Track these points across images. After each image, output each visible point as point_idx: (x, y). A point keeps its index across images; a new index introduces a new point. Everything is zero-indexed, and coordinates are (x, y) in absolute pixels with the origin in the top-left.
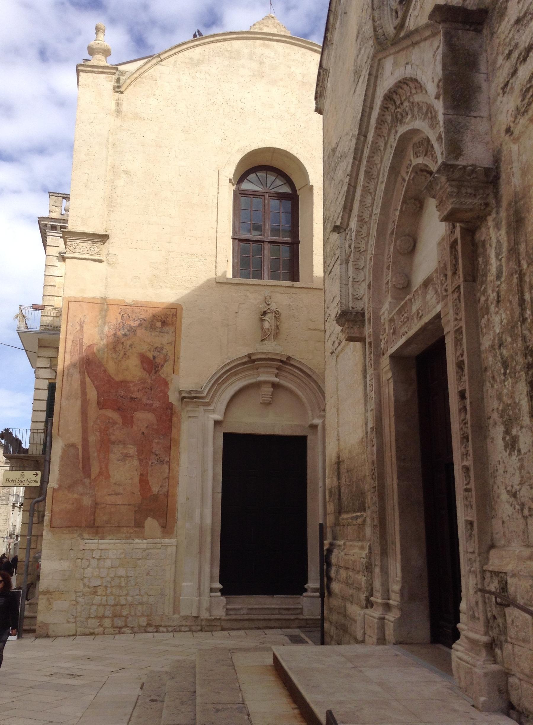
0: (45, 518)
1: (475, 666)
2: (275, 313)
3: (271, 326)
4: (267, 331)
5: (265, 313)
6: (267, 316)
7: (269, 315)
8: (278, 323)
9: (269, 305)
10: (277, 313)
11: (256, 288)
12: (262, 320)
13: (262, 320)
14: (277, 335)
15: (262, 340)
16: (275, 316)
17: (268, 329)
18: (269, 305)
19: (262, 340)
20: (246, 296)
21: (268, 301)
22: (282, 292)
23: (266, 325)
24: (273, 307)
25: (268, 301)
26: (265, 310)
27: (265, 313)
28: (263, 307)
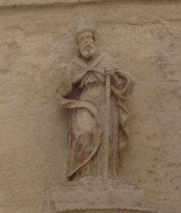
0: (107, 165)
1: (66, 78)
2: (113, 82)
3: (98, 125)
4: (85, 142)
5: (77, 90)
6: (84, 96)
7: (92, 93)
8: (124, 117)
9: (89, 59)
10: (119, 81)
11: (46, 16)
12: (68, 114)
13: (68, 114)
14: (119, 159)
15: (71, 178)
16: (112, 94)
17: (91, 136)
18: (89, 59)
19: (71, 178)
20: (13, 45)
21: (88, 47)
22: (133, 19)
23: (83, 123)
24: (105, 62)
25: (88, 47)
26: (78, 76)
27: (77, 90)
28: (75, 71)
